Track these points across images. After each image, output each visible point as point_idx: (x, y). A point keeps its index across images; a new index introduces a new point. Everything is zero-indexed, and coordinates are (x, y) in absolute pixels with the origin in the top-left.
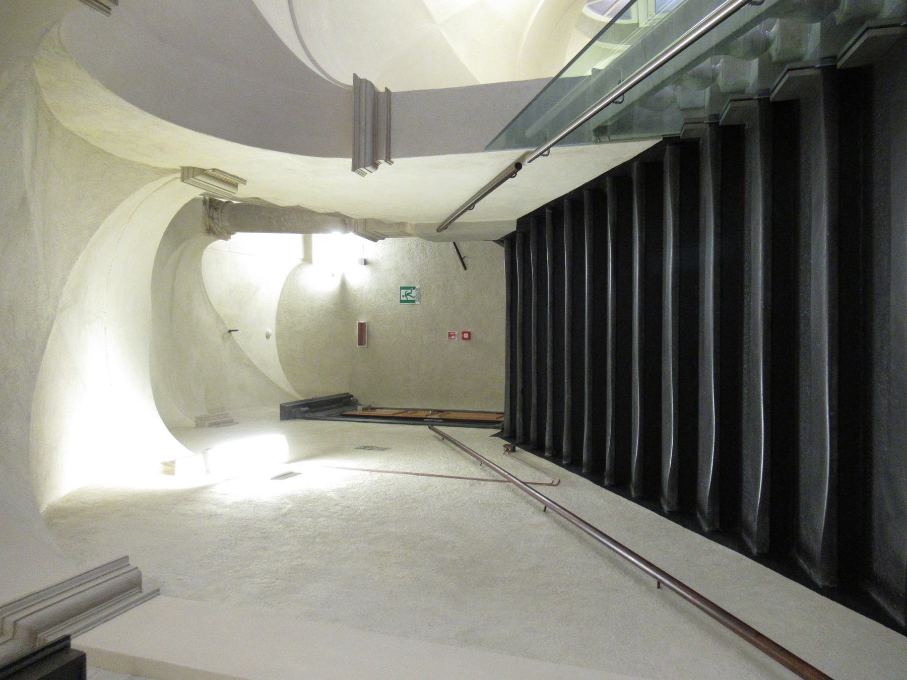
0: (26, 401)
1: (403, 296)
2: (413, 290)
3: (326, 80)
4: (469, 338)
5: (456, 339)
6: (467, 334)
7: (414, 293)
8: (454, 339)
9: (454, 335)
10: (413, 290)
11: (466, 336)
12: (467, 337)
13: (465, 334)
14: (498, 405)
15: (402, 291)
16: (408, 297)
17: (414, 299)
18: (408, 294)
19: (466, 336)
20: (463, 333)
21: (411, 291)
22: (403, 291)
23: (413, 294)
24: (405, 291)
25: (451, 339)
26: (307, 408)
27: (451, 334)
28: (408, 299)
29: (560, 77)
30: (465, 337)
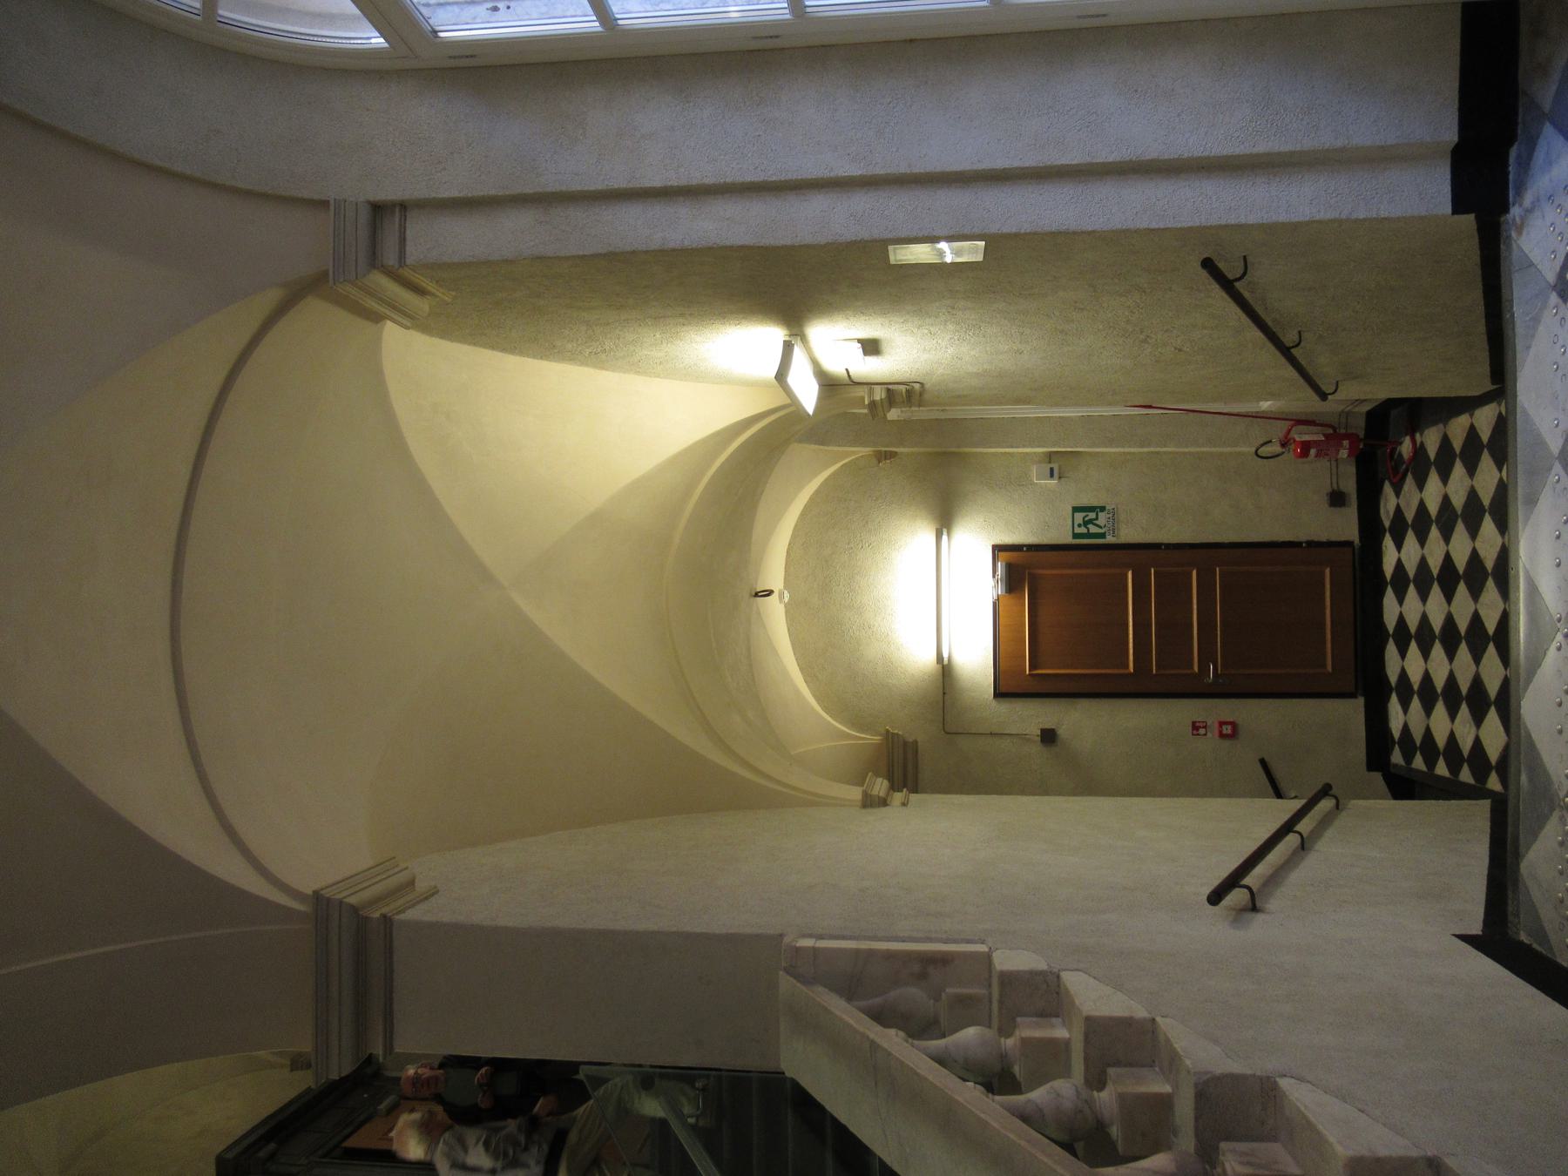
1: (1079, 526)
2: (1100, 514)
3: (850, 462)
4: (1233, 735)
5: (1209, 735)
6: (1229, 727)
7: (1102, 518)
8: (1205, 735)
9: (1205, 727)
10: (1100, 514)
11: (1227, 730)
12: (1229, 732)
13: (1224, 727)
14: (1237, 284)
15: (1076, 515)
16: (1090, 526)
18: (1091, 521)
19: (1227, 730)
20: (1221, 724)
21: (1097, 514)
22: (1079, 517)
24: (1084, 514)
25: (1198, 735)
26: (272, 1146)
27: (1198, 724)
28: (1091, 531)
29: (1303, 802)
30: (1225, 732)
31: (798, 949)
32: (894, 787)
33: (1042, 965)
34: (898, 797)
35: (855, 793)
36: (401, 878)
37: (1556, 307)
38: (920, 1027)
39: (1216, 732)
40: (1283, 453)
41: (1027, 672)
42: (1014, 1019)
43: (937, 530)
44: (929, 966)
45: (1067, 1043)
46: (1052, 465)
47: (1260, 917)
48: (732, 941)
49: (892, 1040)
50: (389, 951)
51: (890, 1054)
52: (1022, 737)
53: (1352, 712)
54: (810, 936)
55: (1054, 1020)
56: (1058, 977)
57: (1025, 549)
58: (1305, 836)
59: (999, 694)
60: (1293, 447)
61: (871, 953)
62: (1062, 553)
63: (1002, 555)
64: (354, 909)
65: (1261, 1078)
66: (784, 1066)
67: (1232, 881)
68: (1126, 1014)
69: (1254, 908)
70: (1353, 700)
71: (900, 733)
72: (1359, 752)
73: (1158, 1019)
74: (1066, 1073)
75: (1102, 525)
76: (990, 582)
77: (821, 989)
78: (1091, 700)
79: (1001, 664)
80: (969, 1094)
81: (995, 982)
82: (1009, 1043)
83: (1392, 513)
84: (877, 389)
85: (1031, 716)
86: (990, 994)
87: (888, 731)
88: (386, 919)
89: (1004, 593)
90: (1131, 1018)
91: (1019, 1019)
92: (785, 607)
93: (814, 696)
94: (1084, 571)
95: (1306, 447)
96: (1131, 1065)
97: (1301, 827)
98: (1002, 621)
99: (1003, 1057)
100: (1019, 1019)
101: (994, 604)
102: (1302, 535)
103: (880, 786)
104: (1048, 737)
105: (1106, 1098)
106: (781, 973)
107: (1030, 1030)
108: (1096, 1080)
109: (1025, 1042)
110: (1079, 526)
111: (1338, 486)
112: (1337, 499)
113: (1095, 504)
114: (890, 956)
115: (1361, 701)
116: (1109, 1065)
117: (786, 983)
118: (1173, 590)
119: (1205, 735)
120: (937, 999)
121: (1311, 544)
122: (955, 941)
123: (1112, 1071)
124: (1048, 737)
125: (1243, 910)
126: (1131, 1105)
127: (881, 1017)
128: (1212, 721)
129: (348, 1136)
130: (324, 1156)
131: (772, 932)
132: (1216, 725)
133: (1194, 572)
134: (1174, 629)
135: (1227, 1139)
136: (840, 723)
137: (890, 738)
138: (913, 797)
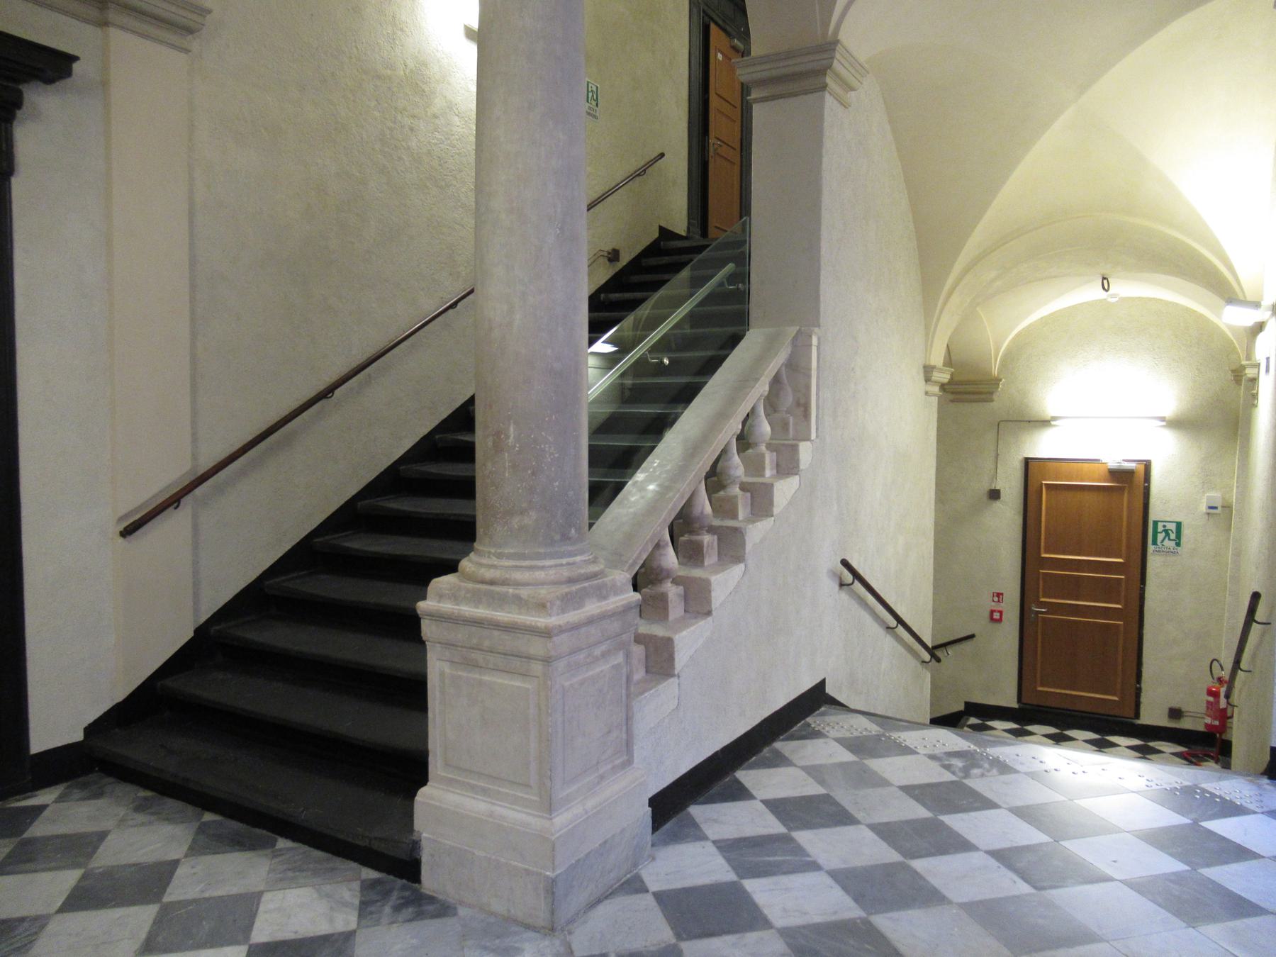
0: (317, 49)
1: (1164, 526)
2: (1174, 542)
4: (992, 619)
5: (993, 604)
7: (1170, 544)
9: (999, 601)
10: (1174, 542)
11: (996, 616)
12: (995, 617)
13: (998, 614)
14: (1254, 624)
15: (1175, 524)
17: (1159, 543)
19: (996, 616)
20: (1001, 612)
21: (1174, 540)
22: (1173, 527)
23: (1167, 542)
24: (1174, 530)
25: (993, 596)
27: (1001, 596)
28: (1159, 535)
30: (995, 614)
31: (811, 336)
32: (943, 387)
33: (802, 467)
34: (936, 389)
35: (937, 358)
36: (854, 82)
37: (1181, 783)
38: (771, 402)
39: (995, 608)
40: (1213, 679)
41: (1043, 482)
42: (774, 451)
43: (1164, 417)
44: (803, 407)
45: (763, 476)
46: (1220, 509)
47: (837, 587)
48: (816, 297)
49: (763, 387)
50: (806, 92)
51: (753, 387)
52: (994, 476)
53: (1009, 699)
54: (819, 343)
55: (775, 471)
56: (796, 474)
57: (1146, 484)
58: (852, 586)
59: (1027, 461)
60: (1217, 685)
61: (809, 377)
62: (1141, 515)
63: (1142, 467)
64: (830, 67)
65: (744, 557)
66: (751, 331)
67: (856, 576)
68: (775, 503)
69: (842, 585)
70: (1016, 700)
71: (999, 389)
72: (979, 698)
73: (773, 518)
74: (747, 473)
75: (1164, 543)
76: (1120, 459)
77: (789, 350)
78: (1021, 526)
79: (1054, 464)
80: (735, 426)
81: (794, 442)
82: (763, 448)
83: (1157, 747)
84: (1255, 371)
85: (1011, 485)
86: (790, 440)
87: (1001, 380)
88: (824, 87)
89: (1109, 467)
90: (773, 505)
91: (775, 454)
92: (1105, 299)
93: (1030, 326)
94: (1125, 524)
95: (1215, 694)
96: (752, 504)
97: (900, 628)
98: (1086, 465)
99: (756, 444)
100: (775, 454)
101: (1099, 460)
102: (1145, 685)
103: (944, 377)
104: (994, 495)
105: (736, 490)
106: (798, 328)
107: (769, 459)
108: (744, 487)
109: (763, 456)
110: (1164, 526)
111: (1187, 716)
112: (1175, 713)
113: (1184, 540)
114: (808, 387)
115: (1015, 705)
116: (751, 494)
117: (792, 331)
118: (1107, 590)
119: (993, 601)
120: (788, 412)
121: (1138, 692)
122: (817, 422)
123: (748, 495)
124: (994, 495)
125: (841, 579)
126: (732, 501)
127: (776, 381)
128: (1002, 606)
129: (716, 23)
130: (704, 12)
131: (821, 320)
132: (1000, 609)
133: (1120, 606)
134: (1075, 587)
135: (719, 539)
136: (1008, 345)
137: (997, 381)
138: (935, 400)
